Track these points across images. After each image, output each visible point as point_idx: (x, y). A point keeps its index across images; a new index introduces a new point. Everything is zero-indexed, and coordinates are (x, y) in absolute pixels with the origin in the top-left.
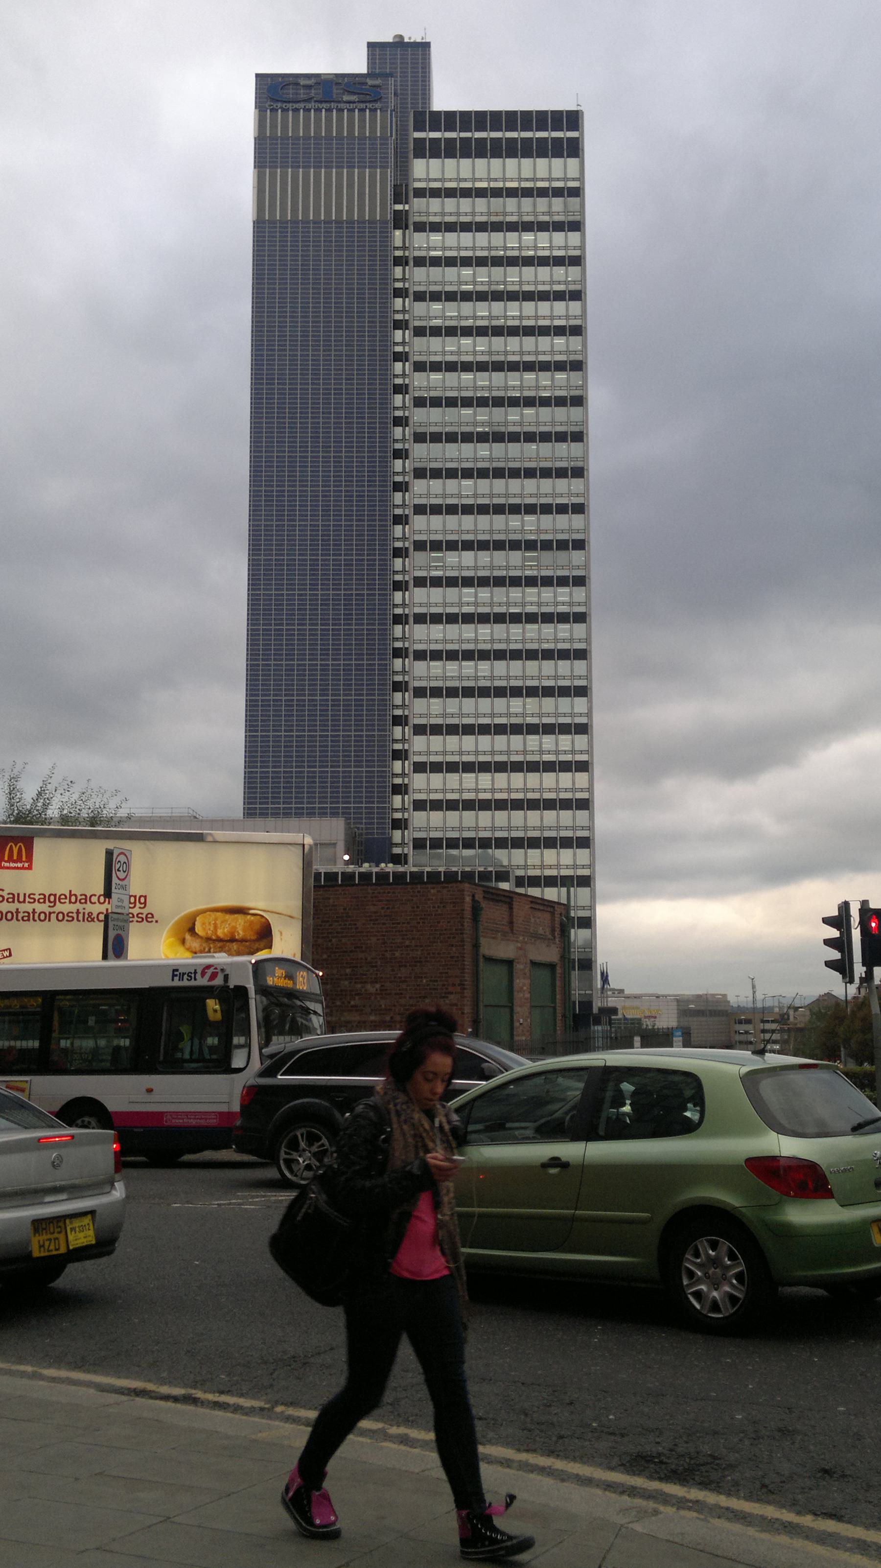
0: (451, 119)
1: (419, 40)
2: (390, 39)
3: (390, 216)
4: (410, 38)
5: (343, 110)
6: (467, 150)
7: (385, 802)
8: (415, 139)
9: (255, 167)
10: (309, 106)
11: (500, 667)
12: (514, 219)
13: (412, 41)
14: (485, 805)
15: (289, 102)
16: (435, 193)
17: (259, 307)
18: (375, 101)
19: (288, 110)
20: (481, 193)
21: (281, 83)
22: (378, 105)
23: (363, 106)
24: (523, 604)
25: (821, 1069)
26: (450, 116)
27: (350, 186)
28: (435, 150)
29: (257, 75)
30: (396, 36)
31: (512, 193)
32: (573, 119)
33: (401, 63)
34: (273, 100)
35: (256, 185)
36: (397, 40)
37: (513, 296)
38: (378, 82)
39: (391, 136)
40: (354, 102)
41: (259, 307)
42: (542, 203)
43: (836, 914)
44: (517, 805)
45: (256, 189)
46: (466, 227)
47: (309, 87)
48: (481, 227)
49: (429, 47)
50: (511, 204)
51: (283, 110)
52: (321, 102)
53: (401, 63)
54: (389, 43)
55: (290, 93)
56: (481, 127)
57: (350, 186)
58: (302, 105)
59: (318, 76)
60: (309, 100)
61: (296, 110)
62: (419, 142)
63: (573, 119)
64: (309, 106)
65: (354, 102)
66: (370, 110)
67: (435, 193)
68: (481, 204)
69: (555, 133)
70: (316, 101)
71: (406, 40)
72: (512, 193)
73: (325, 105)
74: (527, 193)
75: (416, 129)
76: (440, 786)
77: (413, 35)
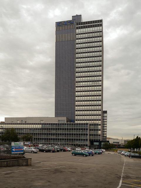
0: (84, 23)
6: (86, 27)
12: (91, 36)
14: (96, 42)
16: (79, 34)
20: (86, 33)
24: (95, 50)
25: (122, 143)
26: (84, 22)
28: (79, 28)
31: (91, 33)
32: (101, 21)
34: (58, 25)
37: (91, 47)
42: (96, 34)
43: (71, 19)
44: (93, 52)
46: (84, 38)
48: (86, 38)
50: (91, 34)
55: (60, 24)
60: (63, 25)
63: (101, 21)
67: (79, 34)
68: (86, 35)
69: (99, 23)
72: (91, 33)
74: (93, 32)
76: (89, 98)
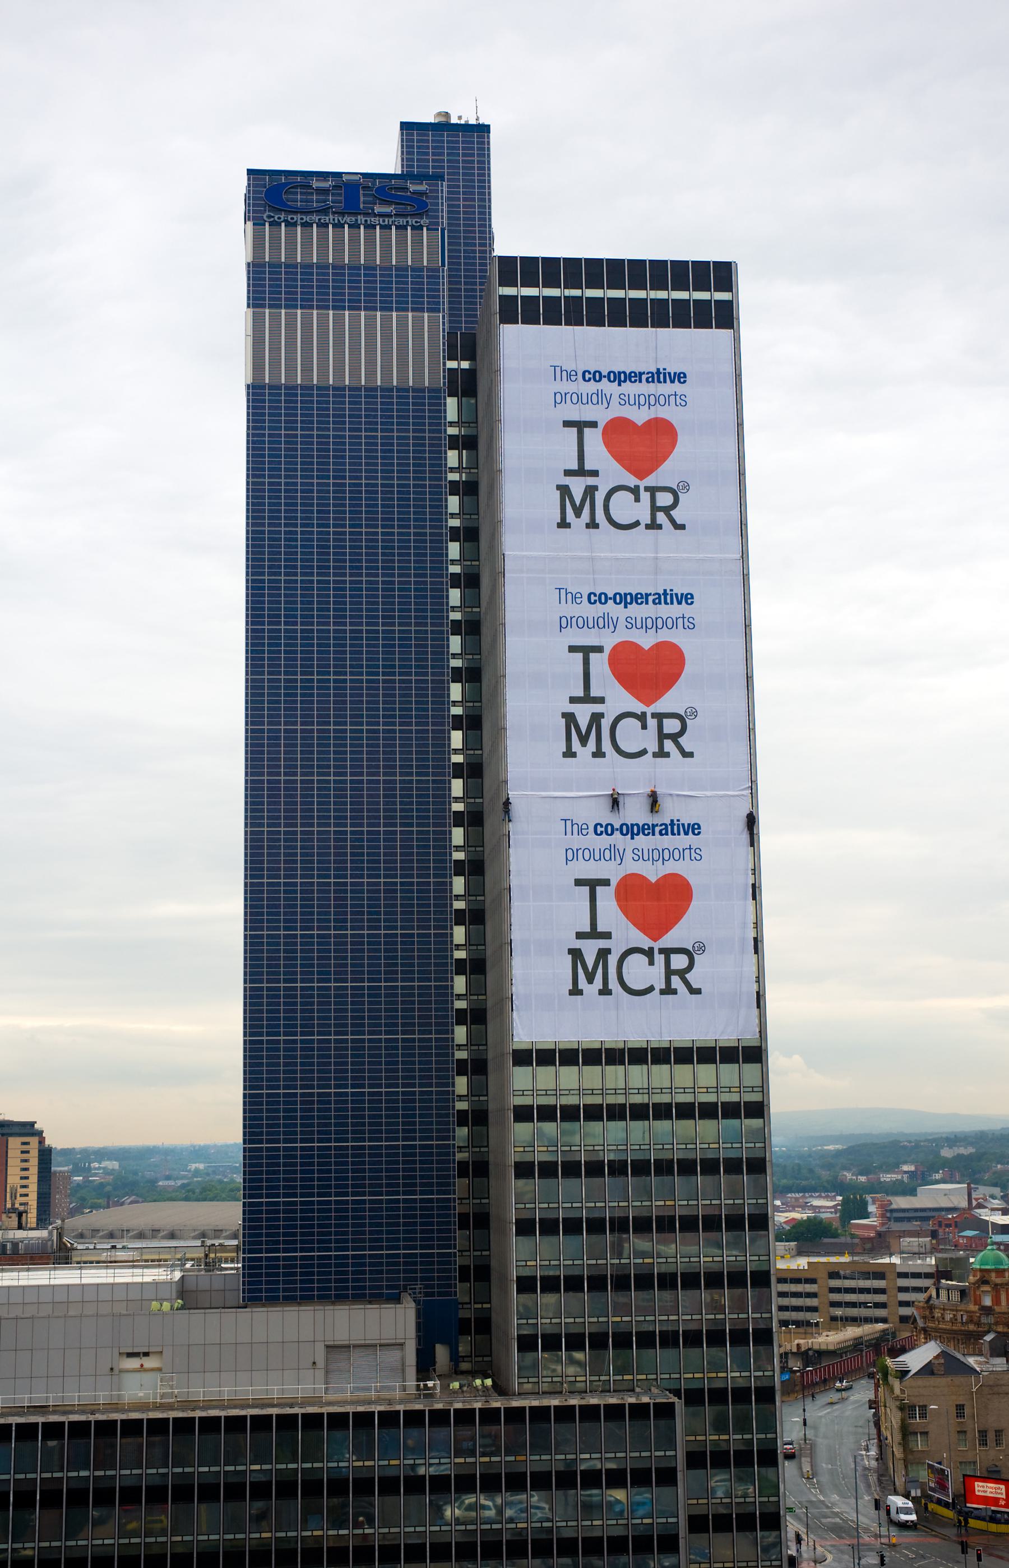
1: (473, 121)
2: (430, 119)
3: (442, 382)
4: (460, 118)
5: (374, 227)
7: (448, 1138)
8: (502, 297)
9: (248, 306)
10: (325, 219)
11: (660, 1074)
13: (463, 122)
15: (296, 213)
17: (257, 497)
18: (420, 215)
19: (295, 224)
21: (286, 184)
22: (425, 221)
23: (402, 221)
27: (387, 338)
29: (250, 172)
30: (439, 114)
32: (722, 274)
33: (448, 157)
34: (273, 209)
35: (250, 332)
36: (442, 119)
38: (423, 187)
39: (443, 265)
40: (389, 216)
41: (257, 497)
45: (250, 340)
47: (320, 191)
49: (489, 132)
51: (288, 224)
52: (343, 214)
53: (448, 157)
54: (431, 124)
56: (595, 283)
57: (387, 338)
58: (315, 218)
59: (338, 175)
60: (324, 211)
61: (307, 225)
62: (507, 301)
63: (722, 274)
64: (325, 219)
65: (389, 216)
66: (413, 228)
70: (334, 213)
71: (454, 120)
73: (348, 219)
75: (502, 284)
77: (462, 113)
